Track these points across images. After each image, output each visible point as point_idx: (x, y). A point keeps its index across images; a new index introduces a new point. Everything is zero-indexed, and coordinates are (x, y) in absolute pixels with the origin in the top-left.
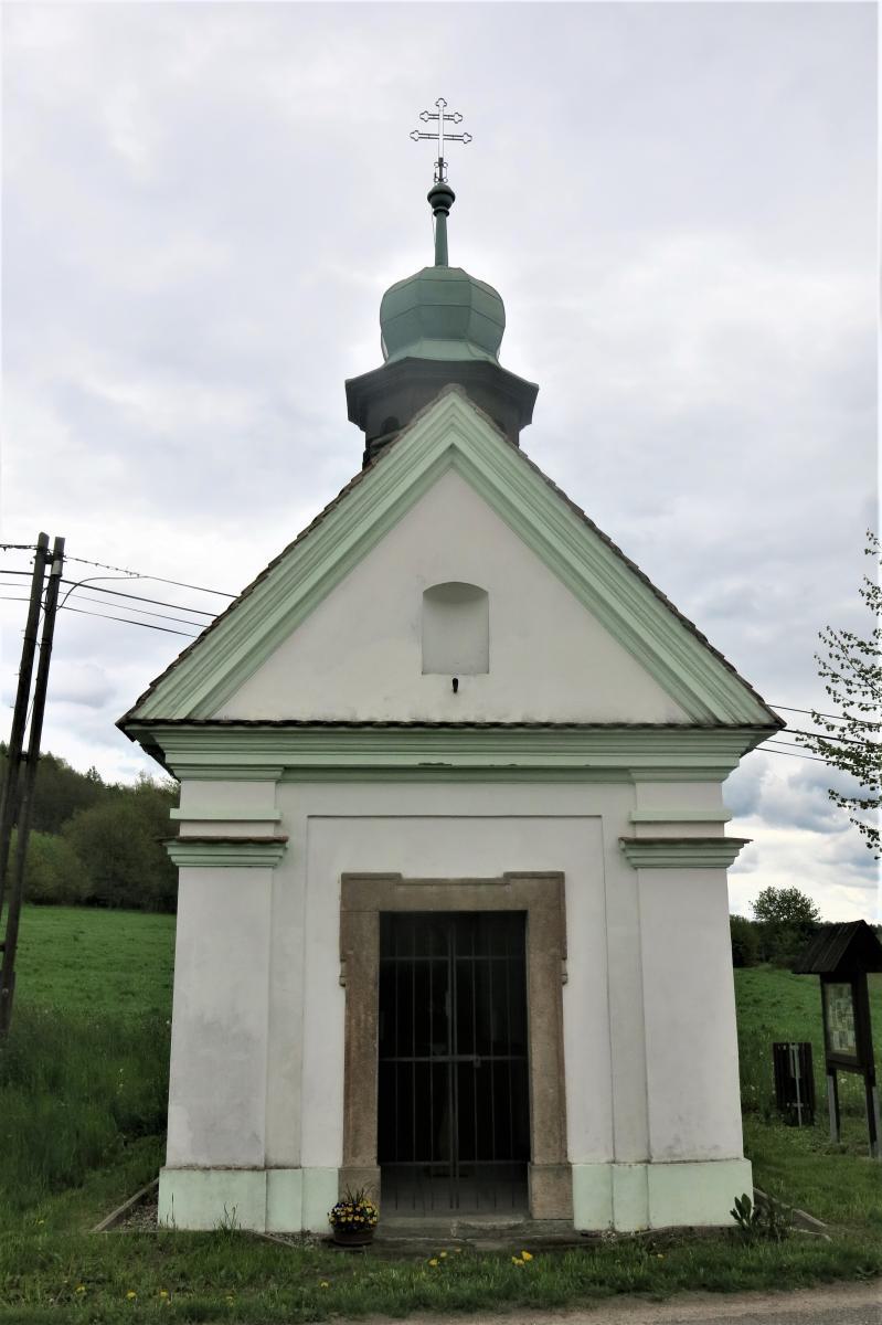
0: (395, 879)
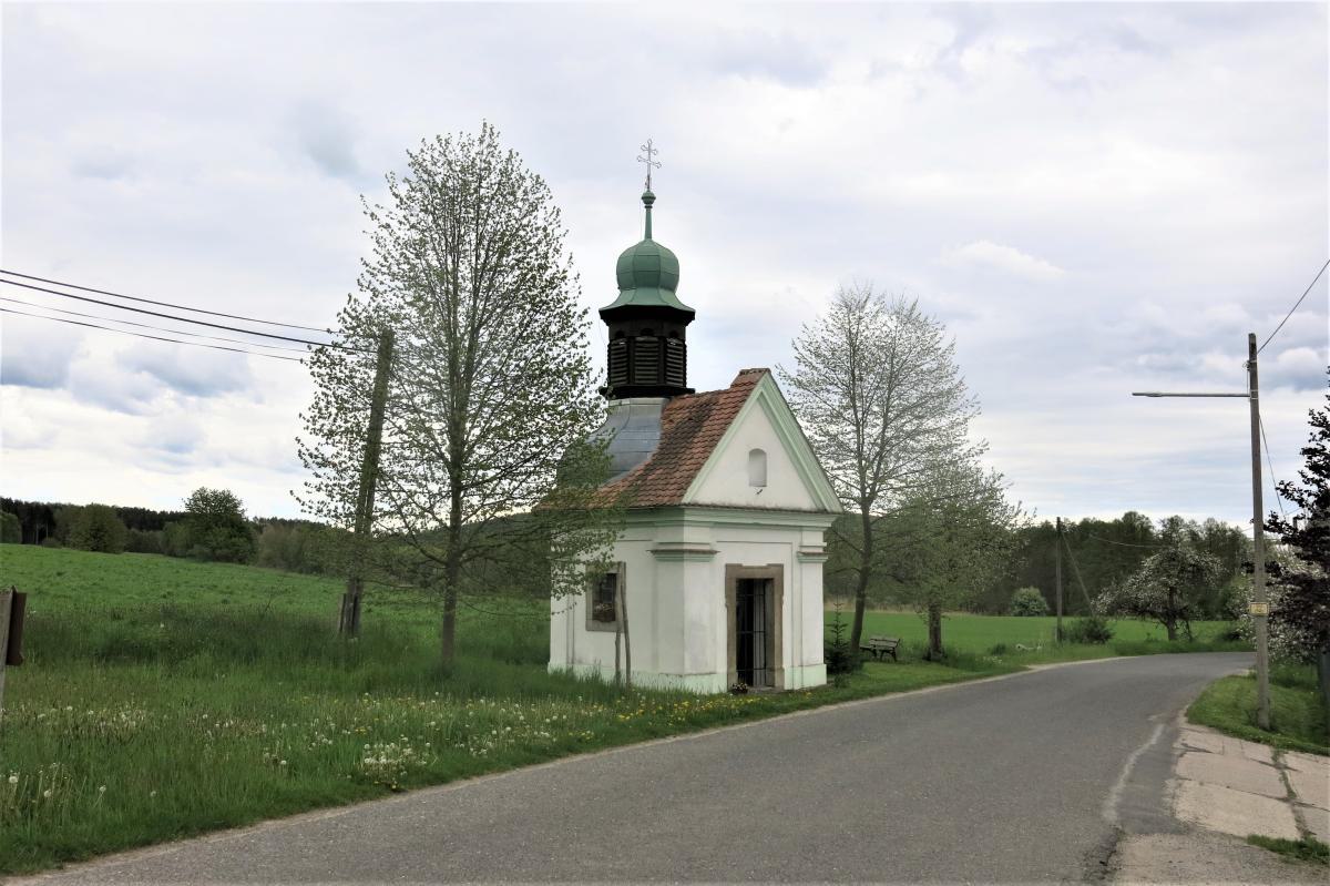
0: (740, 566)
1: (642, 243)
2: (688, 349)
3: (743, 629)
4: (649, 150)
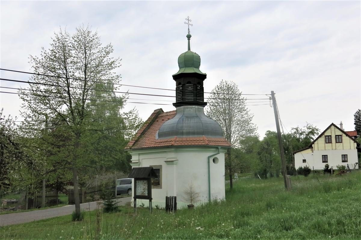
1: (186, 52)
2: (204, 89)
4: (188, 20)
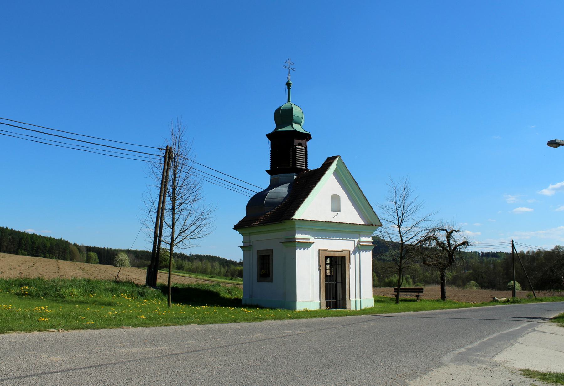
3: (327, 281)
4: (289, 63)
